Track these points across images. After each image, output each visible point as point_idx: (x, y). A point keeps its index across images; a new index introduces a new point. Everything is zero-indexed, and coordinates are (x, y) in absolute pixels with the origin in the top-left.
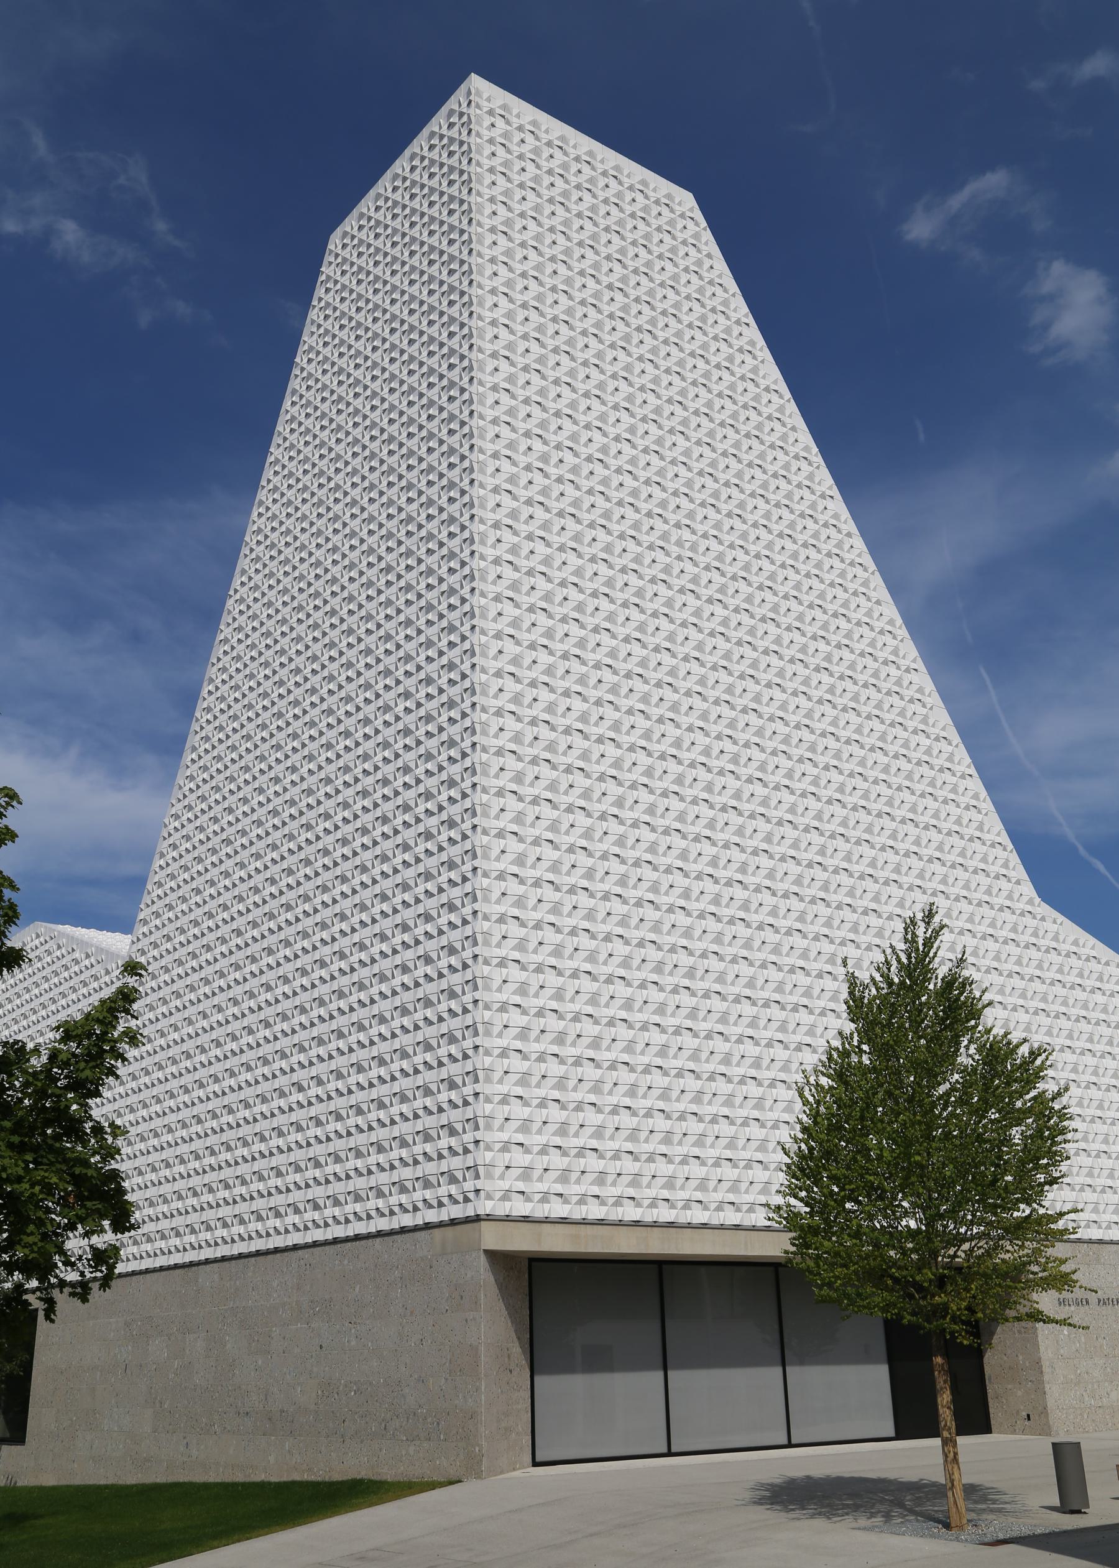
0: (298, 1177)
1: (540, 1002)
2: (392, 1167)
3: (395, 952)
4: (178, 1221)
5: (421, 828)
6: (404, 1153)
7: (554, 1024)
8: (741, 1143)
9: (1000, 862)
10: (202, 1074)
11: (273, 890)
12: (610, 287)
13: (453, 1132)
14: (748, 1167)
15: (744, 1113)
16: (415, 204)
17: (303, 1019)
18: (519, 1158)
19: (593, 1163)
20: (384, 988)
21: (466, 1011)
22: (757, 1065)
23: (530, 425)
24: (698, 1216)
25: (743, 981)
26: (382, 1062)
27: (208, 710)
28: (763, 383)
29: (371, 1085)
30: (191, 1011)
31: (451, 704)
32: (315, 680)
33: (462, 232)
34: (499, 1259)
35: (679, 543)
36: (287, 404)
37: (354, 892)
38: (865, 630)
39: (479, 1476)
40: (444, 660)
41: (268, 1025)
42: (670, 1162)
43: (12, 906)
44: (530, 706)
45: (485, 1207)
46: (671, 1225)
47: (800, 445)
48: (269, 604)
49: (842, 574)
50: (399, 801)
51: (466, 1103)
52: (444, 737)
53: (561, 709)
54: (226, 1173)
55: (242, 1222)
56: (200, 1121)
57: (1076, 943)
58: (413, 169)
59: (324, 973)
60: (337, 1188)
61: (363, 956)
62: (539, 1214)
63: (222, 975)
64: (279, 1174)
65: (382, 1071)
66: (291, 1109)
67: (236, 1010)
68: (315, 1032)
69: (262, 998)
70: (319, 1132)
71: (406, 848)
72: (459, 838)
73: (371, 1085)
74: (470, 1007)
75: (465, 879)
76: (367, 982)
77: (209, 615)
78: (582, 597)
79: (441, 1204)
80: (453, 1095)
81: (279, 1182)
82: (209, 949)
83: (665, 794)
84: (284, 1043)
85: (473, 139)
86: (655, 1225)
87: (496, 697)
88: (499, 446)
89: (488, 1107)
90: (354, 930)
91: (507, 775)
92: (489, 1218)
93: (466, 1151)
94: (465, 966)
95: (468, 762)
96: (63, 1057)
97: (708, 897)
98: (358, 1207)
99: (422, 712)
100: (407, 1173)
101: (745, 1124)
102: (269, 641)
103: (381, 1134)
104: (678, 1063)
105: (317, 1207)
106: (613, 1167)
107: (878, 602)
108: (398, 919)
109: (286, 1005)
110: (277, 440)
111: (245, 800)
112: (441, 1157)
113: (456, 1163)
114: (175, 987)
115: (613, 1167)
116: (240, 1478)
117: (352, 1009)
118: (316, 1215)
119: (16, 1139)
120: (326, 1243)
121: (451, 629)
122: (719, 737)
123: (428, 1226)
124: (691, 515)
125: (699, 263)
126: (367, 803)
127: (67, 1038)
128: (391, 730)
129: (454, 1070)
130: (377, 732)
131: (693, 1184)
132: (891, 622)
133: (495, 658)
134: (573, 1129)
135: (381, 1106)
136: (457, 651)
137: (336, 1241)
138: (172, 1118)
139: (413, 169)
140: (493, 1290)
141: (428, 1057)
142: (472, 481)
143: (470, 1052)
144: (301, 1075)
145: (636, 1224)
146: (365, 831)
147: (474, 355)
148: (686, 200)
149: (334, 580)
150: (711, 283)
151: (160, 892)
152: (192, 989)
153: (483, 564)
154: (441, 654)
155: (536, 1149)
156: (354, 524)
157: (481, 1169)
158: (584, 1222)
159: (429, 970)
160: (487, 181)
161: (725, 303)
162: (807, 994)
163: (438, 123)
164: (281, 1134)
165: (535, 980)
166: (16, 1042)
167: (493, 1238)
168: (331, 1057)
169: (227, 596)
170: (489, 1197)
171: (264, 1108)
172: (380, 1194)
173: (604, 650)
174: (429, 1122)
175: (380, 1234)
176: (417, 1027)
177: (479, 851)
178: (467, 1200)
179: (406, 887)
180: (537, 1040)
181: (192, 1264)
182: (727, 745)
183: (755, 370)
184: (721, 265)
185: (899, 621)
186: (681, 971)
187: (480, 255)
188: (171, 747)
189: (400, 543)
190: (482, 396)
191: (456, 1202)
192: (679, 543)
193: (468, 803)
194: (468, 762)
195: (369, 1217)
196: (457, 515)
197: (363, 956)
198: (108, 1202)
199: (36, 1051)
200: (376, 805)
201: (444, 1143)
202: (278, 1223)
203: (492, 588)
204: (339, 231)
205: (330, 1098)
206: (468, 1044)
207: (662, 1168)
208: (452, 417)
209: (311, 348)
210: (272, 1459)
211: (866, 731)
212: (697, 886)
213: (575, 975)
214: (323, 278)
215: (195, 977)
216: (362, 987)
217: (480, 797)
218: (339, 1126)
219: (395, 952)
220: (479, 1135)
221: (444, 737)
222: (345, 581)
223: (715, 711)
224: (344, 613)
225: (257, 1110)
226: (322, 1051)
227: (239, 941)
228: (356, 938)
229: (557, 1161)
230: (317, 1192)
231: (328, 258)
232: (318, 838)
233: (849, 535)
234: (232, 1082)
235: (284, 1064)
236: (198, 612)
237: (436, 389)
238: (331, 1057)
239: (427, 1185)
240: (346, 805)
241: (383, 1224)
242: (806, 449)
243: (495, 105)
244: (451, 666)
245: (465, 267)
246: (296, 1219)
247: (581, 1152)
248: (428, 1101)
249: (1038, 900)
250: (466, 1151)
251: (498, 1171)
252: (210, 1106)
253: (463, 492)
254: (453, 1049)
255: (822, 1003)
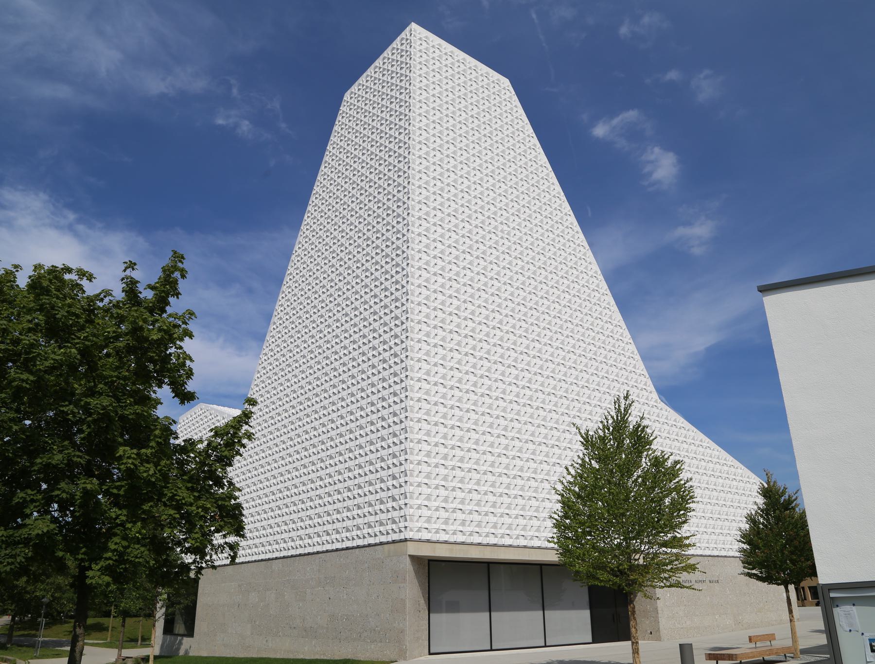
0: (319, 520)
1: (436, 440)
2: (365, 516)
3: (367, 415)
4: (263, 540)
5: (381, 357)
6: (371, 509)
7: (442, 450)
8: (527, 508)
9: (643, 383)
10: (274, 488)
11: (310, 387)
12: (472, 116)
13: (394, 500)
14: (530, 519)
15: (529, 494)
16: (384, 102)
17: (323, 447)
18: (426, 512)
19: (460, 516)
20: (362, 432)
21: (401, 443)
22: (535, 472)
23: (435, 174)
24: (507, 541)
25: (529, 433)
26: (360, 467)
27: (282, 305)
28: (540, 163)
29: (355, 478)
30: (271, 443)
31: (397, 300)
32: (330, 321)
33: (405, 143)
34: (415, 559)
35: (502, 231)
36: (322, 167)
37: (348, 388)
38: (584, 275)
39: (405, 659)
40: (394, 280)
41: (306, 450)
42: (495, 516)
43: (191, 370)
44: (433, 302)
45: (409, 535)
46: (495, 545)
47: (556, 191)
48: (309, 284)
49: (574, 250)
50: (371, 345)
51: (401, 486)
52: (393, 315)
53: (448, 304)
54: (286, 518)
55: (293, 540)
56: (274, 494)
57: (675, 420)
58: (384, 63)
59: (333, 426)
60: (338, 525)
61: (352, 417)
62: (434, 539)
63: (285, 427)
64: (311, 519)
65: (361, 471)
66: (317, 489)
67: (291, 443)
68: (328, 453)
69: (302, 454)
70: (330, 499)
71: (373, 404)
72: (399, 343)
73: (355, 478)
74: (403, 441)
75: (402, 381)
76: (354, 430)
77: (279, 282)
78: (458, 253)
79: (388, 533)
80: (395, 482)
81: (311, 522)
82: (278, 430)
83: (494, 345)
84: (314, 458)
85: (411, 101)
86: (488, 545)
87: (417, 333)
88: (421, 183)
89: (412, 488)
90: (348, 405)
91: (423, 333)
92: (411, 540)
93: (401, 508)
94: (401, 422)
95: (404, 327)
96: (214, 444)
97: (514, 394)
98: (348, 534)
99: (382, 304)
100: (372, 519)
101: (529, 499)
102: (309, 301)
103: (359, 500)
104: (499, 470)
105: (328, 534)
106: (469, 518)
107: (590, 263)
108: (369, 400)
109: (315, 441)
110: (317, 183)
111: (297, 361)
112: (388, 511)
113: (395, 514)
114: (263, 433)
115: (469, 518)
116: (291, 656)
117: (346, 442)
118: (328, 538)
119: (190, 485)
120: (333, 551)
121: (397, 265)
122: (519, 320)
123: (381, 544)
124: (507, 219)
125: (511, 109)
126: (355, 346)
127: (216, 435)
128: (368, 312)
129: (395, 470)
130: (361, 313)
131: (505, 526)
132: (596, 272)
133: (418, 279)
134: (450, 500)
135: (360, 487)
136: (400, 275)
137: (337, 550)
138: (261, 492)
139: (384, 63)
140: (413, 574)
141: (383, 464)
142: (409, 198)
143: (403, 462)
144: (322, 473)
145: (479, 544)
146: (354, 359)
147: (411, 142)
148: (506, 82)
149: (340, 274)
150: (517, 118)
151: (257, 389)
152: (271, 433)
153: (413, 235)
154: (392, 277)
155: (434, 508)
156: (350, 263)
157: (408, 517)
158: (455, 543)
159: (384, 424)
160: (418, 134)
161: (523, 127)
162: (558, 440)
163: (396, 43)
164: (312, 500)
165: (434, 429)
166: (190, 439)
167: (413, 549)
168: (336, 465)
169: (291, 254)
170: (411, 530)
171: (304, 488)
172: (359, 528)
173: (469, 329)
174: (383, 495)
175: (358, 547)
176: (377, 451)
177: (409, 368)
178: (400, 531)
179: (373, 385)
180: (435, 457)
181: (269, 559)
182: (523, 324)
183: (536, 157)
184: (521, 111)
185: (599, 272)
186: (501, 427)
187: (414, 112)
188: (260, 338)
189: (372, 274)
190: (414, 160)
191: (395, 532)
192: (502, 231)
193: (404, 346)
194: (404, 327)
195: (353, 539)
196: (400, 263)
197: (352, 417)
198: (232, 518)
199: (201, 441)
200: (360, 347)
201: (390, 505)
202: (310, 541)
203: (417, 247)
204: (349, 92)
205: (335, 483)
206: (402, 458)
207: (492, 519)
208: (399, 200)
209: (334, 142)
210: (306, 648)
211: (585, 321)
212: (509, 389)
213: (452, 428)
214: (341, 112)
215: (273, 428)
216: (351, 432)
217: (409, 363)
218: (339, 497)
219: (367, 415)
220: (407, 501)
221: (393, 315)
222: (346, 260)
223: (518, 308)
224: (345, 290)
225: (300, 489)
226: (332, 462)
227: (294, 411)
228: (349, 409)
229: (443, 514)
230: (329, 527)
231: (344, 103)
232: (332, 363)
233: (577, 232)
234: (289, 476)
235: (314, 468)
236: (273, 279)
237: (392, 187)
238: (336, 465)
239: (381, 524)
240: (345, 348)
241: (360, 542)
242: (559, 193)
243: (422, 36)
244: (397, 282)
245: (407, 146)
246: (319, 539)
247: (454, 510)
248: (382, 485)
249: (659, 401)
250: (401, 508)
251: (416, 518)
252: (279, 487)
253: (404, 235)
254: (395, 461)
255: (565, 445)
